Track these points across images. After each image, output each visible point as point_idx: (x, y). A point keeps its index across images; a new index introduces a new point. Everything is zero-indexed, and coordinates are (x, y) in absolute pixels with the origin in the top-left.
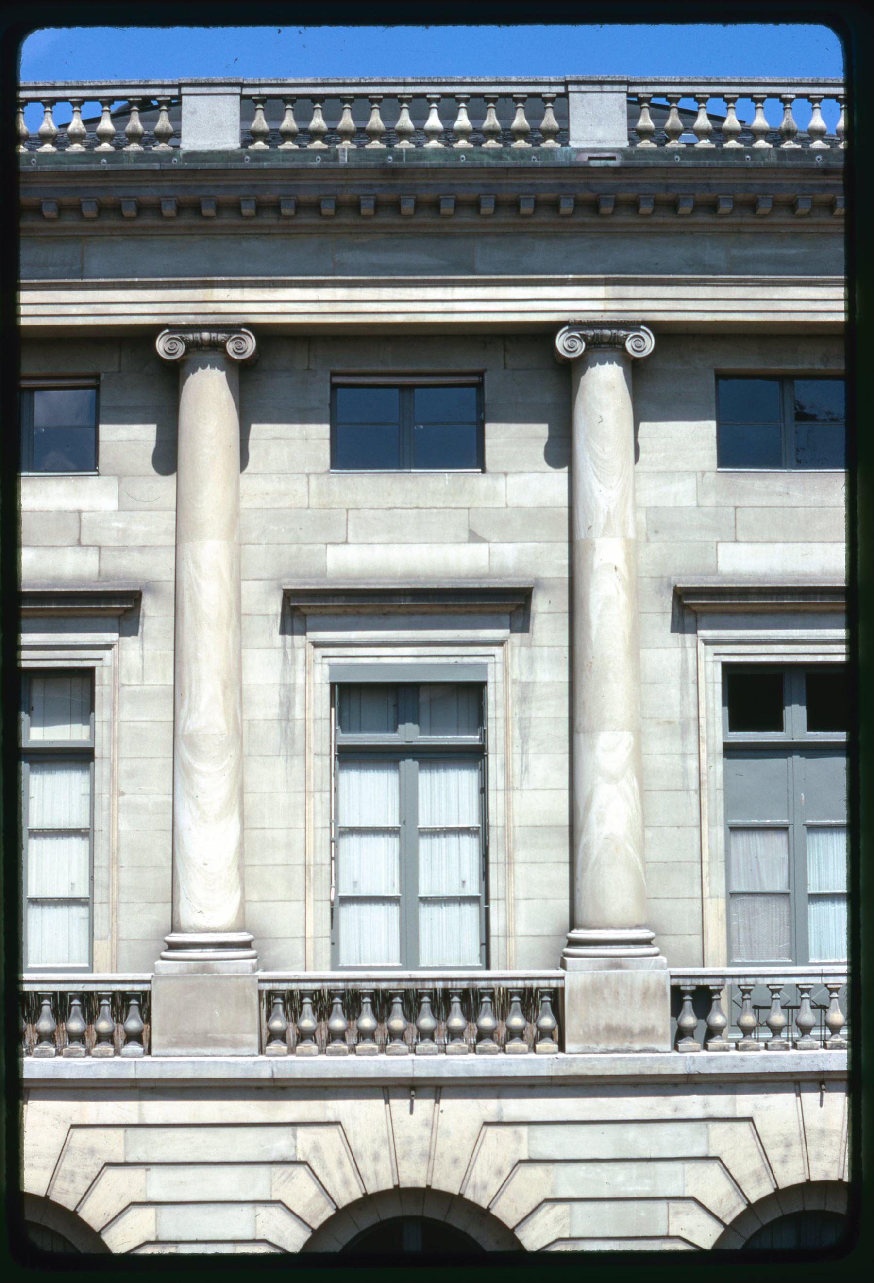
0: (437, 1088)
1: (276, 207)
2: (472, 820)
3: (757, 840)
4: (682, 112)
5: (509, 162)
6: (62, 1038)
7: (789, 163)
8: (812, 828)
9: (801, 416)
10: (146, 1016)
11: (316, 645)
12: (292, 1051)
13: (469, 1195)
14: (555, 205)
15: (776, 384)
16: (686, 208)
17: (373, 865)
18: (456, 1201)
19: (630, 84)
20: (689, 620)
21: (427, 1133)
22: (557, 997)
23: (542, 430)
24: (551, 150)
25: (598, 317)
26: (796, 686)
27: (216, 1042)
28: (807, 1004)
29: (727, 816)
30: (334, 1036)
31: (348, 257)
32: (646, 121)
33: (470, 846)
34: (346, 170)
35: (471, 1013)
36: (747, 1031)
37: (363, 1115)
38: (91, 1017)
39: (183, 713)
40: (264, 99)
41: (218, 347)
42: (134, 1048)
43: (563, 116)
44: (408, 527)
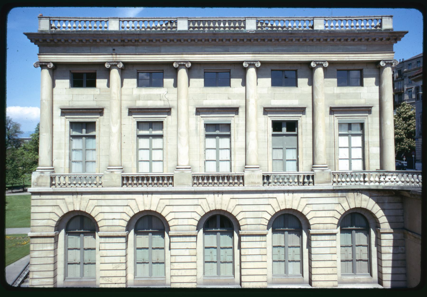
0: (223, 192)
1: (194, 40)
2: (229, 147)
3: (277, 150)
4: (266, 24)
5: (235, 32)
6: (158, 184)
7: (285, 32)
8: (287, 148)
9: (286, 78)
10: (243, 179)
11: (202, 117)
12: (198, 186)
13: (228, 211)
14: (243, 40)
15: (281, 72)
16: (266, 41)
17: (211, 155)
18: (226, 212)
19: (257, 18)
20: (266, 113)
21: (221, 200)
22: (243, 177)
23: (241, 80)
24: (242, 30)
25: (319, 60)
26: (285, 124)
27: (185, 185)
28: (286, 178)
29: (272, 146)
30: (205, 184)
31: (207, 49)
32: (259, 25)
33: (228, 151)
34: (207, 34)
35: (228, 180)
36: (275, 183)
37: (69, 198)
38: (163, 180)
39: (179, 129)
40: (192, 21)
41: (184, 65)
42: (171, 186)
43: (245, 24)
44: (217, 97)
